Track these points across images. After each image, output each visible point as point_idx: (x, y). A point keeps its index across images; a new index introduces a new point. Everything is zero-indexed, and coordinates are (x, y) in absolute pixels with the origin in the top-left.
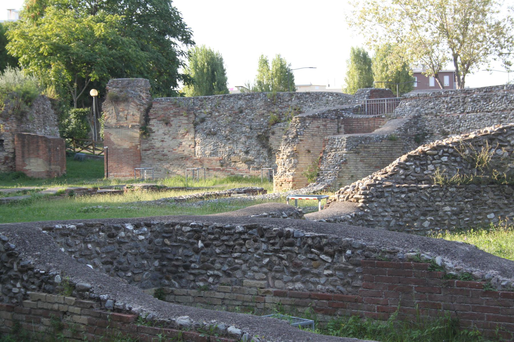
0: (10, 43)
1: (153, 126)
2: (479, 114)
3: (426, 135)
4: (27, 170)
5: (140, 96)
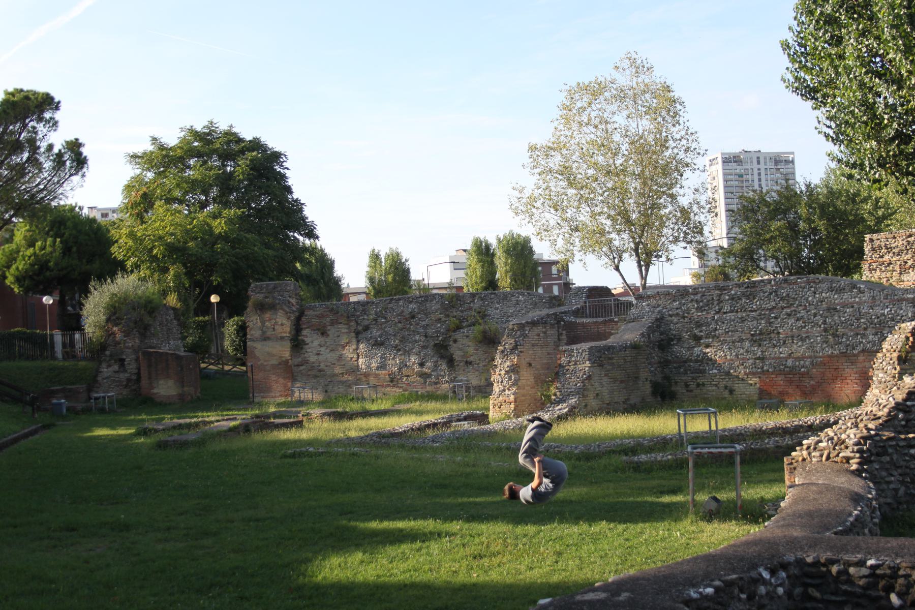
0: (116, 245)
1: (306, 336)
2: (740, 315)
3: (672, 340)
4: (154, 394)
5: (289, 302)
